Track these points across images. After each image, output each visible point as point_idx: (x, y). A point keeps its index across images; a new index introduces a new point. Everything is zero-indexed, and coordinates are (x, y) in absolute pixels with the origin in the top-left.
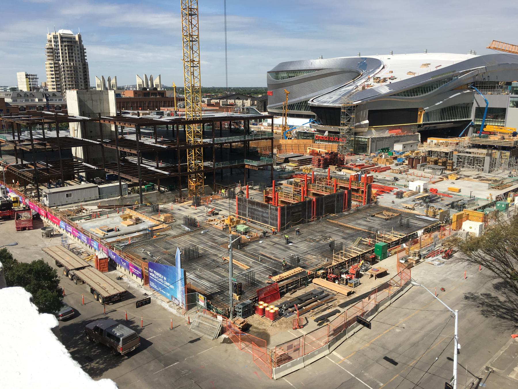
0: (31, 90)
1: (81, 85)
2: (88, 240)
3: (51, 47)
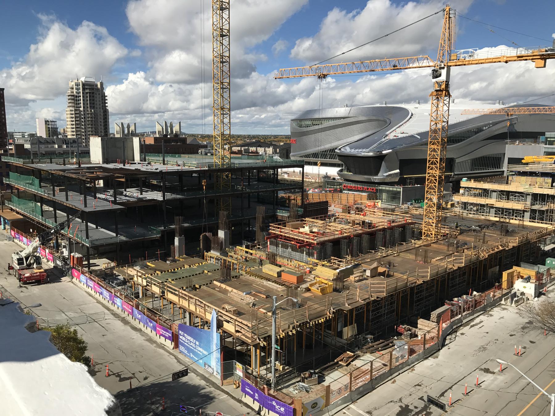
0: (49, 137)
1: (101, 132)
2: (110, 296)
3: (72, 94)
